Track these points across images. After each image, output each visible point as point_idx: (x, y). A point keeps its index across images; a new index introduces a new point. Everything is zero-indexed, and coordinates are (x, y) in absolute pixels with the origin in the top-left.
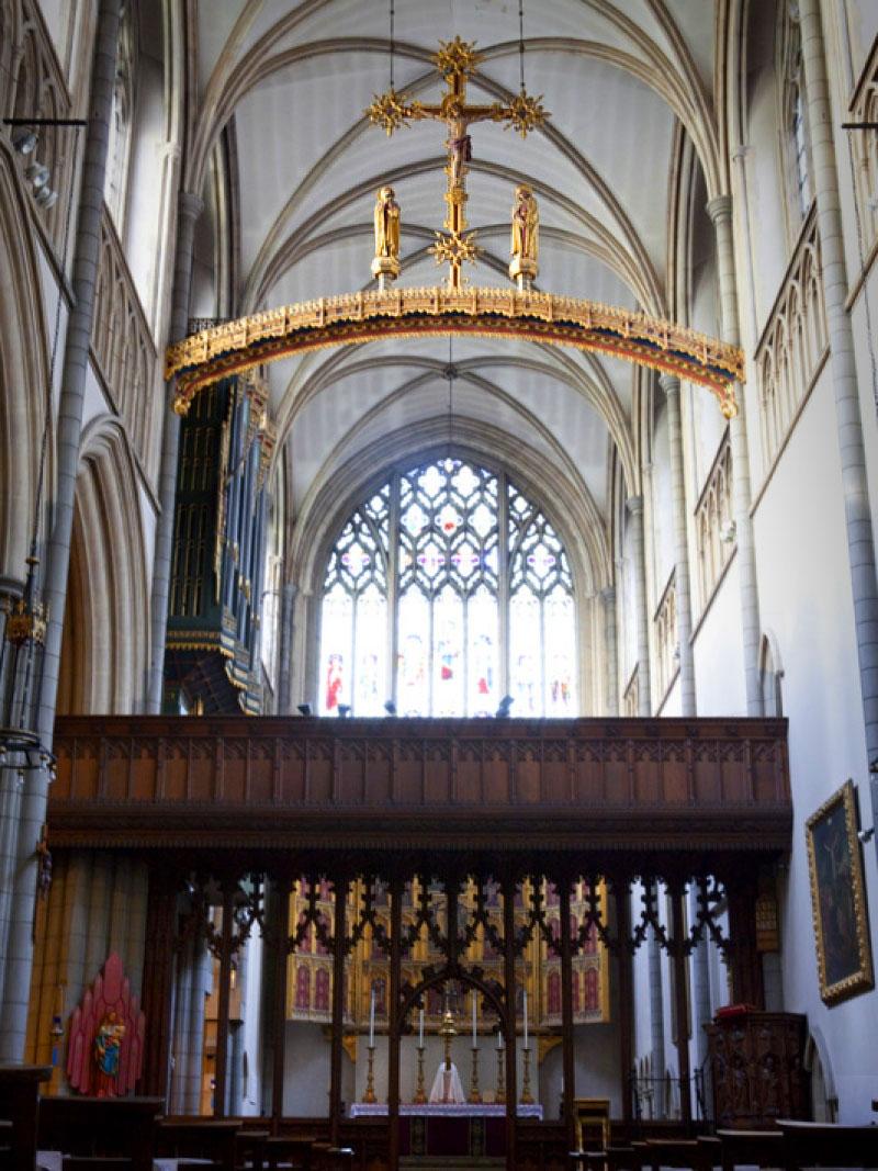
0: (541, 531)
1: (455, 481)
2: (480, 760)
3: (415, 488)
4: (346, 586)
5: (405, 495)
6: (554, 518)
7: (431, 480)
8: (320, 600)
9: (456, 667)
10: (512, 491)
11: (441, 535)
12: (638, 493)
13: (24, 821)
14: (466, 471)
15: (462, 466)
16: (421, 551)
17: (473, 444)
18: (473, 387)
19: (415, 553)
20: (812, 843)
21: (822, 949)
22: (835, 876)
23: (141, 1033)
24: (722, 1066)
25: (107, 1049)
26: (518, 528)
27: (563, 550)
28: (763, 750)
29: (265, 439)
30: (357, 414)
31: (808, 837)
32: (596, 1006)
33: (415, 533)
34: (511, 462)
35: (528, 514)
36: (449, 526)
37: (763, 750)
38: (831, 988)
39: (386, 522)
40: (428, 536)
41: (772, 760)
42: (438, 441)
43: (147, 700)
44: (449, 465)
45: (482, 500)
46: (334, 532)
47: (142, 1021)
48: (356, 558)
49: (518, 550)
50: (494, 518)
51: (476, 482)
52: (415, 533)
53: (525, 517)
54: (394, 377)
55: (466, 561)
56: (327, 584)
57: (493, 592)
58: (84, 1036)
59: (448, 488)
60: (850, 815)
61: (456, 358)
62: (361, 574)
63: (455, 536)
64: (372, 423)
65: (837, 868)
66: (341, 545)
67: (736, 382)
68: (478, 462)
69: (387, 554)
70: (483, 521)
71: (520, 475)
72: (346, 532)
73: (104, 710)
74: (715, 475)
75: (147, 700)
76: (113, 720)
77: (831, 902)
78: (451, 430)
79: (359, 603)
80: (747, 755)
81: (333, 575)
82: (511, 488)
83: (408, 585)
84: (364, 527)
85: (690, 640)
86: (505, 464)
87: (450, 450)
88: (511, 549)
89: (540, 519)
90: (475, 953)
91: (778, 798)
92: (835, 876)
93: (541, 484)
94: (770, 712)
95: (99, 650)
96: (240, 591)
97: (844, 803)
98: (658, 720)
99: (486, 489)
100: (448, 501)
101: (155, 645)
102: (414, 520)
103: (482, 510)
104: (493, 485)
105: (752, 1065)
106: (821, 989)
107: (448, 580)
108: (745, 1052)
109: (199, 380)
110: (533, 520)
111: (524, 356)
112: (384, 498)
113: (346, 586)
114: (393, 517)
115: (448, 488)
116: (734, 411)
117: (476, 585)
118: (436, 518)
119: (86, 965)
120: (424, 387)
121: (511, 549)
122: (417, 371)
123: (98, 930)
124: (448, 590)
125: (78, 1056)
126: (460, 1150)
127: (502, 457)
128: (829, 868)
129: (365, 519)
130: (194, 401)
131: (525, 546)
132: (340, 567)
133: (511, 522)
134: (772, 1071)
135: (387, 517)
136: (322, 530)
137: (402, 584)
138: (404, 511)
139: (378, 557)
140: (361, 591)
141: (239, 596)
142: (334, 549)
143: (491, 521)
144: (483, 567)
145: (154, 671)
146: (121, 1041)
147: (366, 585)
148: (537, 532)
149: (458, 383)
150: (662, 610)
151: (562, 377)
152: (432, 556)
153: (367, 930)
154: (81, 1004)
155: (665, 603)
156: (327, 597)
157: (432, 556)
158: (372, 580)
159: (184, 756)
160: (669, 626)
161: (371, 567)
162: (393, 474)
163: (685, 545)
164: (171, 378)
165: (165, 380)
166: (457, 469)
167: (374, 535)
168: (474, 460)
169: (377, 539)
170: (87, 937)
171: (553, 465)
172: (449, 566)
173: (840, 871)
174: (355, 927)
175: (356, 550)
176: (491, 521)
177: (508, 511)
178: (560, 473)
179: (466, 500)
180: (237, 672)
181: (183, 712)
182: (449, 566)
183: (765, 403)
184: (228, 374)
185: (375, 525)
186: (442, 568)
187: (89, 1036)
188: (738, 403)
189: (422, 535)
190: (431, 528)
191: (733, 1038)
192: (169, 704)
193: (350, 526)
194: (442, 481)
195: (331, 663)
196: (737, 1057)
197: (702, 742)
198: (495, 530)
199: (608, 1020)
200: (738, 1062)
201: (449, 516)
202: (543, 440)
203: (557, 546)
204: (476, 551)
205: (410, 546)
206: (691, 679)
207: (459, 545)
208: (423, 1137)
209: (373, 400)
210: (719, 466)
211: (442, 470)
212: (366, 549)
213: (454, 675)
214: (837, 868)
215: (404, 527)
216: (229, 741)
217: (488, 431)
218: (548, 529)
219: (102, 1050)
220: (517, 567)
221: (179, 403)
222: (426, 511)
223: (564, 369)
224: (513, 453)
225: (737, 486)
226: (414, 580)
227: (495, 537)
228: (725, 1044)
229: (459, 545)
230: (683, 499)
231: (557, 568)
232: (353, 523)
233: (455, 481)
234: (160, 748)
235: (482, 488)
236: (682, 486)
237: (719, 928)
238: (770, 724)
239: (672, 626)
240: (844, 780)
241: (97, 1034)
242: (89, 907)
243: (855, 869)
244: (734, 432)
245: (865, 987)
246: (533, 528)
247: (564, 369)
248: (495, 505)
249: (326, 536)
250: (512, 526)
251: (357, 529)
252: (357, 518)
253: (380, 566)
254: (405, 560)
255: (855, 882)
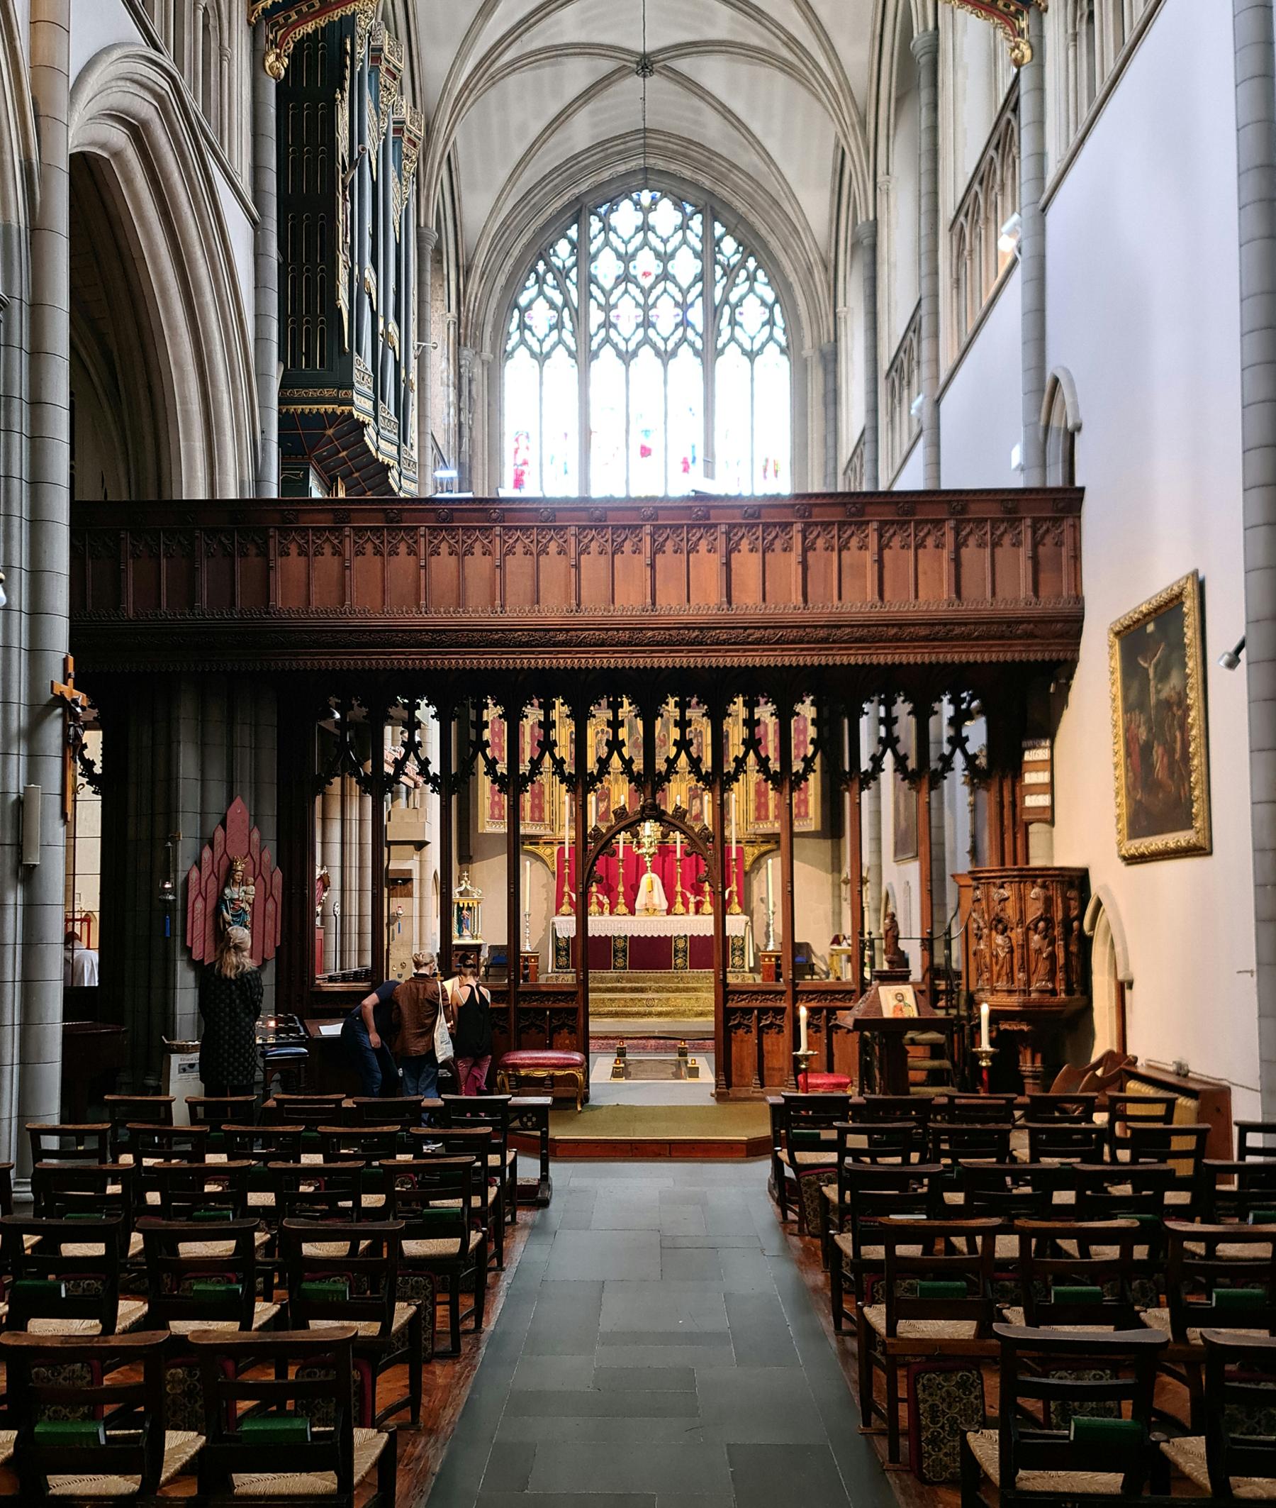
0: (752, 278)
1: (653, 218)
2: (307, 555)
3: (607, 228)
4: (530, 349)
5: (595, 237)
6: (769, 263)
7: (625, 216)
8: (501, 368)
9: (654, 443)
10: (719, 229)
11: (638, 285)
12: (871, 217)
13: (35, 652)
14: (666, 205)
15: (661, 198)
16: (615, 306)
17: (673, 167)
18: (678, 88)
19: (607, 308)
20: (1118, 656)
21: (1123, 792)
22: (1153, 701)
23: (278, 893)
24: (979, 928)
25: (232, 915)
26: (725, 274)
27: (776, 301)
28: (1047, 531)
29: (406, 134)
30: (536, 128)
31: (1111, 647)
32: (807, 814)
33: (608, 283)
34: (718, 190)
35: (738, 256)
36: (646, 274)
37: (1047, 531)
38: (1137, 842)
39: (575, 270)
40: (622, 287)
41: (1058, 544)
42: (632, 165)
43: (259, 480)
44: (646, 197)
45: (684, 241)
46: (514, 285)
47: (278, 876)
48: (540, 316)
49: (726, 301)
50: (698, 263)
51: (677, 218)
52: (608, 283)
53: (734, 260)
54: (578, 74)
55: (665, 315)
56: (509, 348)
57: (697, 353)
58: (205, 899)
59: (645, 227)
60: (1191, 622)
61: (651, 46)
62: (547, 336)
63: (653, 287)
64: (552, 140)
65: (1158, 692)
66: (523, 300)
67: (1032, 10)
68: (682, 194)
69: (577, 311)
70: (686, 267)
71: (727, 205)
72: (528, 284)
73: (201, 494)
74: (984, 166)
75: (259, 480)
76: (214, 506)
77: (1143, 734)
78: (646, 150)
79: (544, 368)
80: (1027, 537)
81: (515, 337)
82: (717, 225)
83: (600, 346)
84: (549, 277)
85: (936, 397)
86: (711, 194)
87: (647, 177)
88: (717, 301)
89: (751, 263)
90: (677, 794)
91: (1065, 594)
92: (1153, 701)
93: (753, 218)
94: (1055, 479)
95: (186, 412)
96: (380, 338)
97: (1182, 603)
98: (889, 494)
99: (688, 227)
100: (645, 243)
101: (264, 407)
102: (606, 268)
103: (685, 255)
104: (696, 224)
105: (1019, 930)
106: (1119, 843)
107: (646, 340)
108: (1011, 912)
109: (296, 24)
110: (742, 264)
111: (739, 39)
112: (571, 241)
113: (530, 349)
114: (582, 264)
115: (645, 227)
116: (1028, 53)
117: (678, 345)
118: (631, 264)
119: (203, 813)
120: (612, 90)
121: (717, 301)
122: (607, 66)
123: (216, 772)
124: (646, 351)
125: (198, 929)
126: (665, 964)
127: (707, 183)
128: (1144, 690)
129: (550, 267)
130: (293, 58)
131: (733, 298)
132: (523, 326)
133: (718, 268)
134: (1045, 938)
135: (575, 265)
136: (501, 280)
137: (594, 346)
138: (593, 258)
139: (566, 312)
140: (548, 355)
141: (381, 345)
142: (517, 306)
143: (696, 266)
144: (684, 323)
145: (265, 440)
146: (252, 905)
147: (553, 348)
148: (748, 279)
149: (654, 81)
150: (898, 362)
151: (785, 67)
152: (627, 314)
153: (888, 761)
154: (198, 863)
155: (902, 354)
156: (509, 363)
157: (627, 314)
158: (560, 341)
159: (302, 552)
160: (905, 382)
161: (558, 326)
162: (580, 210)
163: (935, 273)
164: (258, 21)
165: (249, 23)
166: (654, 202)
167: (560, 287)
168: (675, 190)
169: (564, 292)
170: (203, 781)
171: (766, 192)
172: (647, 324)
173: (1163, 695)
174: (599, 760)
175: (541, 305)
176: (696, 266)
177: (714, 253)
178: (776, 202)
179: (665, 241)
180: (382, 444)
181: (316, 494)
182: (647, 324)
183: (1075, 36)
184: (336, 15)
185: (562, 274)
186: (638, 326)
187: (211, 903)
188: (1033, 41)
189: (615, 286)
190: (626, 278)
191: (996, 897)
192: (292, 482)
193: (533, 276)
194: (638, 218)
195: (517, 440)
196: (1000, 921)
197: (969, 520)
198: (700, 278)
199: (819, 828)
200: (1000, 927)
201: (646, 264)
202: (756, 159)
203: (770, 296)
204: (677, 304)
205: (602, 300)
206: (936, 444)
207: (658, 298)
208: (624, 951)
209: (554, 109)
210: (992, 152)
211: (637, 204)
212: (552, 305)
213: (653, 453)
214: (1158, 692)
215: (596, 277)
216: (359, 531)
217: (689, 149)
218: (760, 274)
219: (228, 917)
220: (724, 323)
221: (271, 58)
222: (619, 256)
223: (785, 53)
224: (720, 179)
225: (1025, 167)
226: (607, 340)
227: (699, 286)
228: (984, 902)
229: (658, 298)
230: (934, 210)
231: (770, 322)
232: (537, 273)
233: (653, 218)
234: (271, 542)
235: (684, 227)
236: (934, 193)
237: (699, 759)
238: (1060, 496)
239: (909, 383)
240: (1188, 570)
241: (221, 900)
242: (203, 747)
243: (1193, 697)
244: (1024, 85)
245: (1200, 850)
246: (743, 274)
247: (785, 53)
248: (699, 247)
249: (506, 288)
250: (719, 271)
251: (540, 281)
252: (541, 267)
253: (568, 325)
254: (596, 317)
255: (1193, 714)
